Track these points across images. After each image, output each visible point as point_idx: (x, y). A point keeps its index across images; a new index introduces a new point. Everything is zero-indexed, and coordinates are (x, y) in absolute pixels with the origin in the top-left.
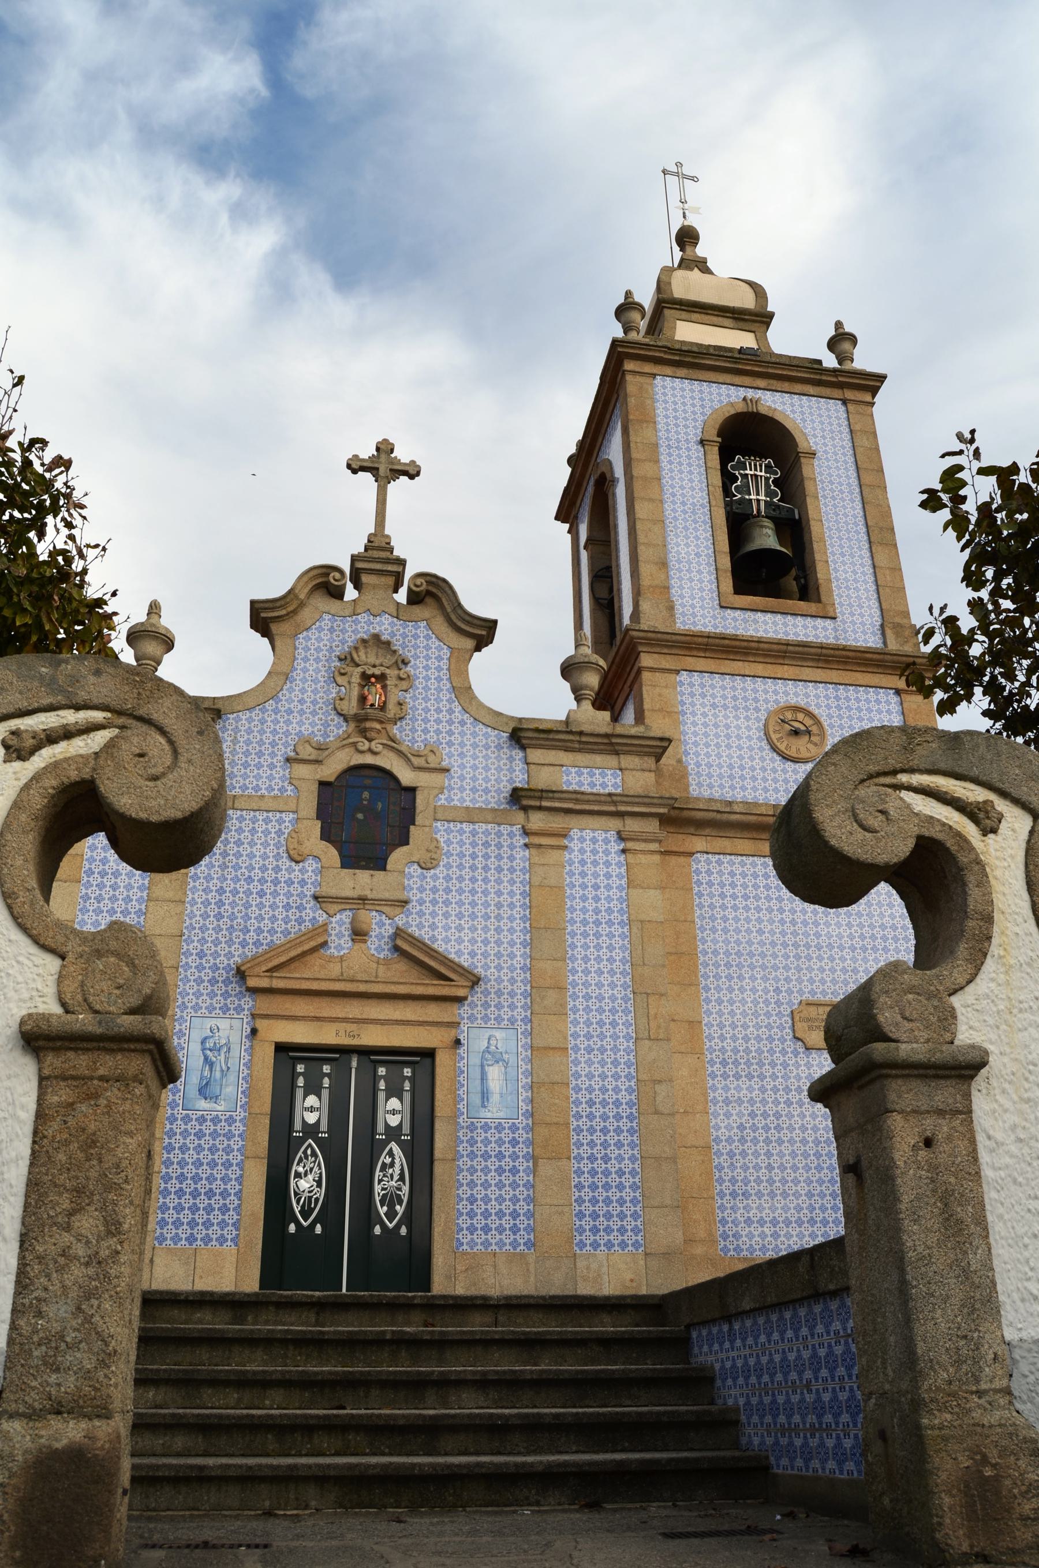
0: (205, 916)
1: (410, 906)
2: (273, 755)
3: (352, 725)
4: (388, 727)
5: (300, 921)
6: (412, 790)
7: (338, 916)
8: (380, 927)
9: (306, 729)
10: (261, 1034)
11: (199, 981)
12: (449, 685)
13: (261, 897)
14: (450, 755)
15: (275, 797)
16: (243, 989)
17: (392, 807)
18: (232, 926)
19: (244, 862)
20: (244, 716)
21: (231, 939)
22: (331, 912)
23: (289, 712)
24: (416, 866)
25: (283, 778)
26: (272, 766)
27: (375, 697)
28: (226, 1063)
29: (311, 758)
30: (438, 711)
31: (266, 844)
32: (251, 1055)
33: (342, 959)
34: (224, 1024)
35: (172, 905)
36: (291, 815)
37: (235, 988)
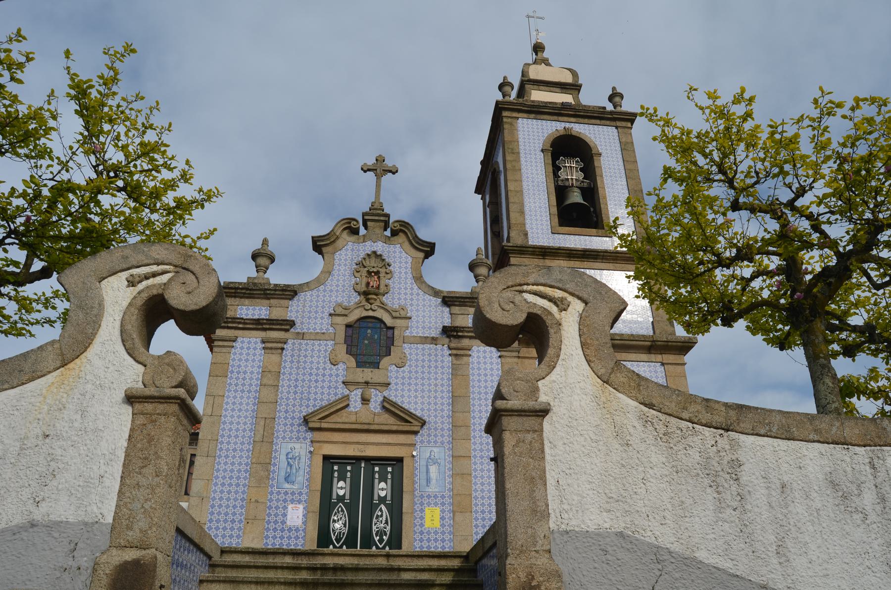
2: (323, 312)
5: (336, 394)
8: (376, 397)
9: (340, 300)
11: (285, 425)
26: (322, 318)
27: (374, 283)
31: (319, 357)
33: (356, 413)
34: (297, 446)
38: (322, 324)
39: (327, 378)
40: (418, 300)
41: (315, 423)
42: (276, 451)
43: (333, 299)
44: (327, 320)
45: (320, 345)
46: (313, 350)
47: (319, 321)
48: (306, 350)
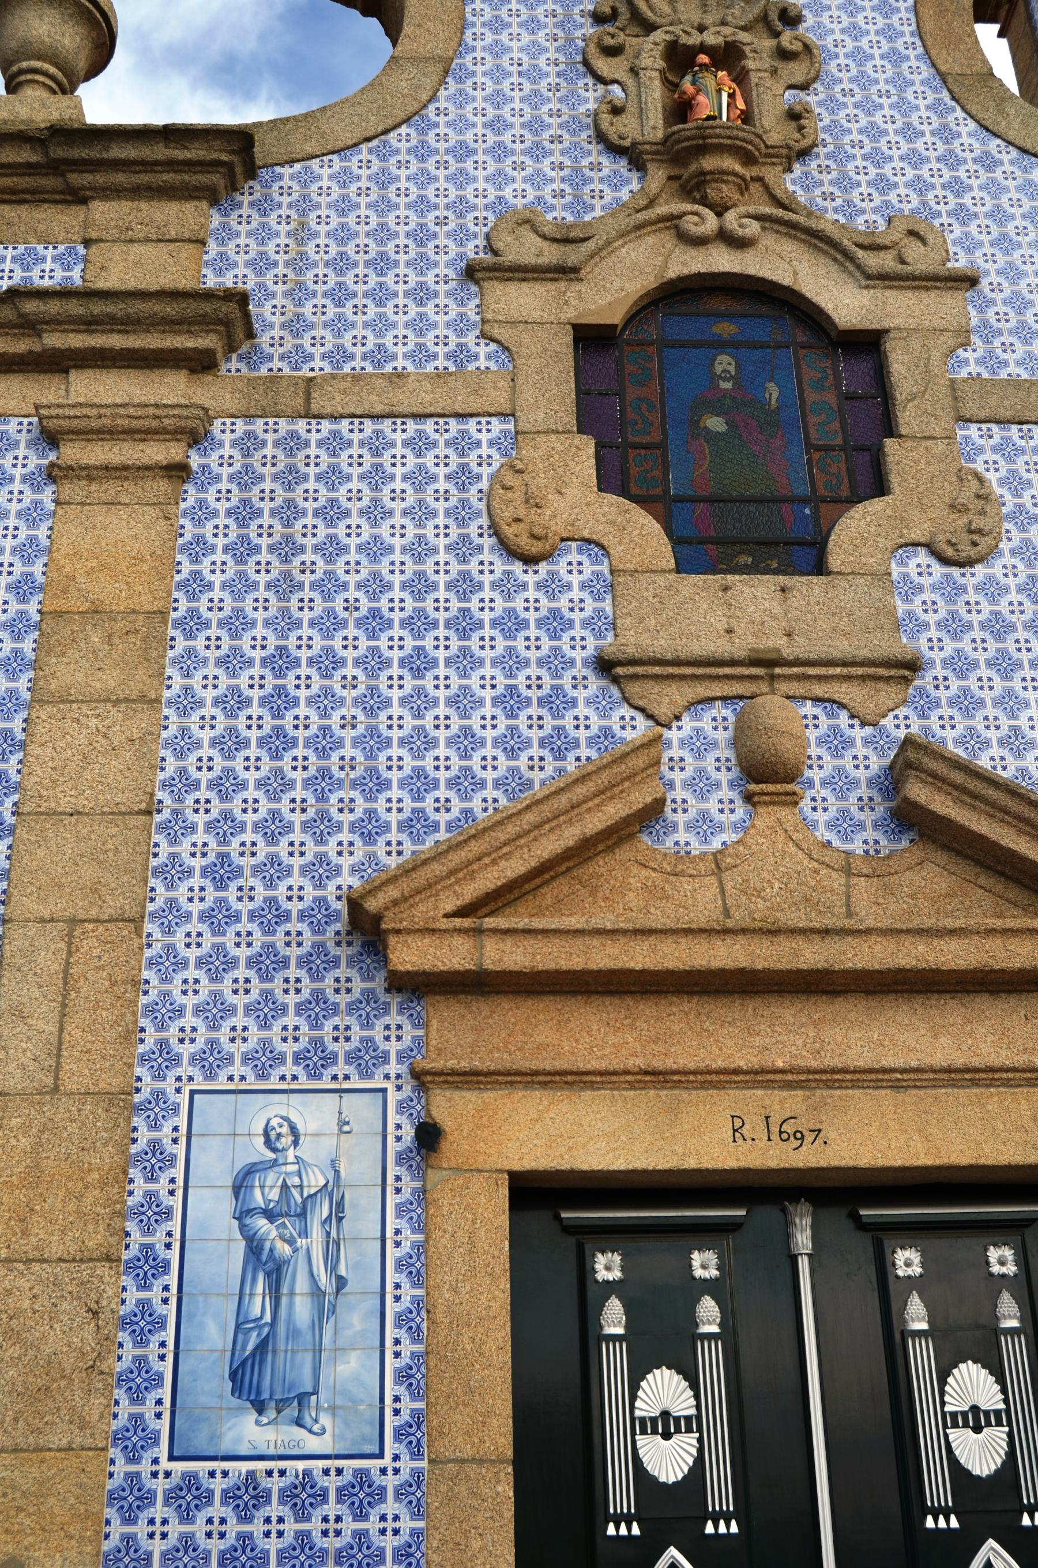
0: (230, 743)
1: (925, 680)
2: (422, 264)
3: (658, 176)
4: (770, 174)
5: (558, 744)
6: (867, 345)
7: (688, 723)
8: (841, 756)
9: (519, 193)
10: (456, 1144)
11: (218, 964)
12: (926, 71)
13: (418, 673)
14: (971, 246)
15: (441, 376)
16: (379, 983)
17: (811, 396)
18: (324, 773)
19: (352, 569)
20: (325, 170)
21: (323, 816)
22: (663, 711)
23: (462, 152)
24: (923, 557)
25: (459, 325)
26: (421, 294)
27: (715, 98)
28: (332, 1262)
29: (544, 260)
30: (910, 133)
31: (421, 513)
32: (422, 1226)
33: (718, 864)
34: (314, 1115)
35: (114, 714)
36: (496, 425)
37: (348, 979)
38: (421, 325)
39: (489, 644)
40: (994, 189)
41: (440, 956)
42: (157, 1159)
43: (481, 190)
44: (449, 310)
45: (335, 444)
46: (377, 477)
47: (401, 312)
48: (333, 477)
